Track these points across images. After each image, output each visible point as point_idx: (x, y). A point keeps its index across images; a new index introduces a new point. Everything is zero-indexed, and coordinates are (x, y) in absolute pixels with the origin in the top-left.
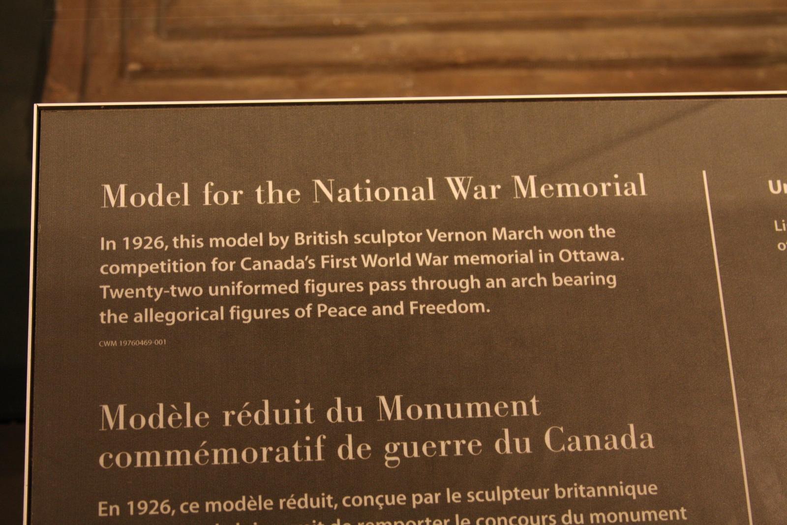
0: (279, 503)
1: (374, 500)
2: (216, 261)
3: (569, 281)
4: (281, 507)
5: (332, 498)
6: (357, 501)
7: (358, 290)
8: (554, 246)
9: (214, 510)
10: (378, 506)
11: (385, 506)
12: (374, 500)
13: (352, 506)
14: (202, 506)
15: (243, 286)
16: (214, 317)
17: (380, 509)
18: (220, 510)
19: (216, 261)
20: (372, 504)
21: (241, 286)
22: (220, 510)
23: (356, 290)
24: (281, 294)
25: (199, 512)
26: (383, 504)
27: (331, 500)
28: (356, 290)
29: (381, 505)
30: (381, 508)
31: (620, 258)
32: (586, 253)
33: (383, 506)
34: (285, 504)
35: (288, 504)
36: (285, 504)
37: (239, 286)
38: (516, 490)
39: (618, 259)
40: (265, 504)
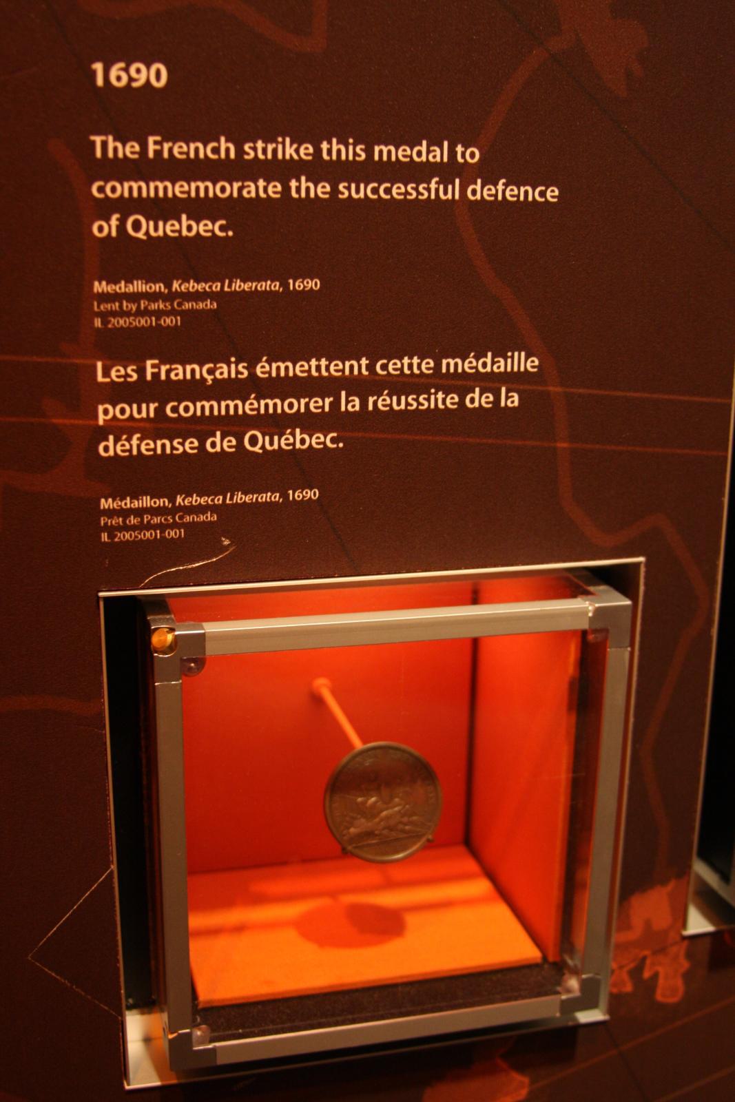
0: (441, 363)
1: (201, 371)
2: (138, 439)
3: (405, 153)
4: (371, 408)
5: (368, 362)
6: (187, 409)
7: (409, 197)
8: (159, 427)
9: (271, 411)
10: (206, 380)
11: (215, 380)
12: (201, 371)
13: (107, 197)
14: (438, 365)
15: (141, 442)
16: (222, 373)
17: (208, 384)
18: (279, 411)
19: (138, 439)
20: (198, 376)
21: (138, 442)
22: (279, 411)
23: (405, 197)
24: (119, 456)
25: (493, 406)
26: (212, 377)
27: (367, 365)
28: (405, 197)
29: (209, 378)
30: (210, 382)
31: (279, 288)
32: (215, 366)
33: (212, 380)
34: (375, 403)
35: (380, 403)
36: (375, 403)
37: (135, 442)
38: (261, 183)
39: (277, 288)
40: (529, 364)
